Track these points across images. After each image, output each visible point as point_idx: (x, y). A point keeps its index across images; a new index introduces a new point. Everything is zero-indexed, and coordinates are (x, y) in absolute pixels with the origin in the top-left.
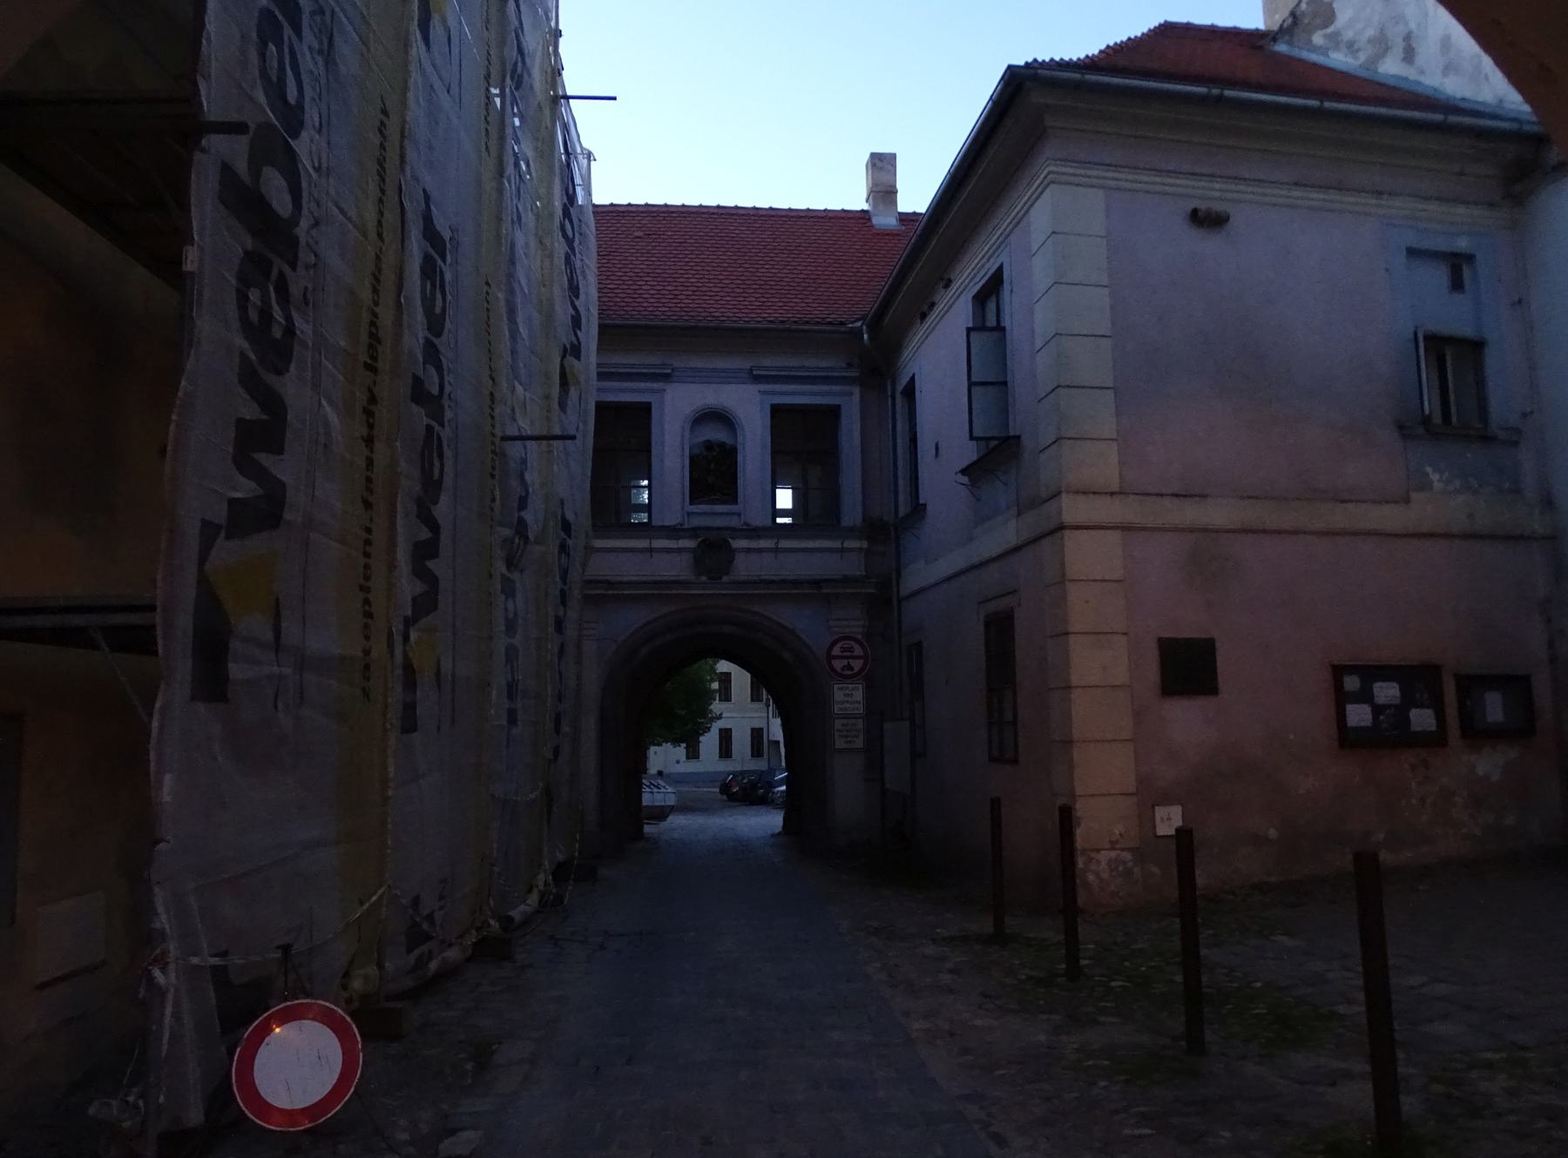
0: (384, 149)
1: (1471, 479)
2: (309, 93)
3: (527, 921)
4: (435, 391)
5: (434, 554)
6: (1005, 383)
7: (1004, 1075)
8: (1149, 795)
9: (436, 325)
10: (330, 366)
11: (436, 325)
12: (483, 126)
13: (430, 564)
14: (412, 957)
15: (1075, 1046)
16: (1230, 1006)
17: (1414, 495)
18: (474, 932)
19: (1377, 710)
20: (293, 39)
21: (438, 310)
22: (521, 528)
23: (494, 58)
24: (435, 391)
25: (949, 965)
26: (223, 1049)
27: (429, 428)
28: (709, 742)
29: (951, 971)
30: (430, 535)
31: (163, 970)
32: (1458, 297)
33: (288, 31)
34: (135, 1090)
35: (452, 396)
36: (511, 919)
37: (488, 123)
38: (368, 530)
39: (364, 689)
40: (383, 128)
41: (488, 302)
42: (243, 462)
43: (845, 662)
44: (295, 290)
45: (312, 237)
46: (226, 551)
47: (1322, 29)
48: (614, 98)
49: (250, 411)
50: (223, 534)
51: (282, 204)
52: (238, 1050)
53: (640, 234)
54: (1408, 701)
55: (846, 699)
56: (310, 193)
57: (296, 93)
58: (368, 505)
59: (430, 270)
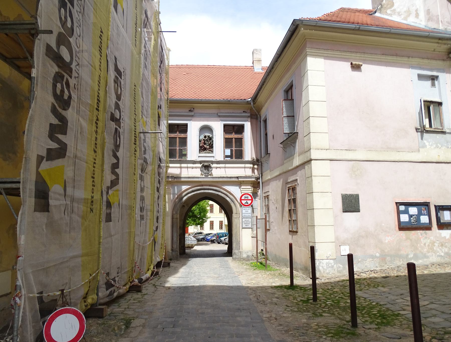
0: (102, 43)
1: (438, 144)
2: (75, 24)
3: (147, 280)
4: (118, 118)
5: (118, 167)
6: (294, 116)
7: (292, 333)
8: (339, 243)
9: (119, 97)
10: (84, 109)
11: (119, 97)
12: (134, 38)
13: (116, 170)
14: (108, 292)
15: (316, 324)
16: (365, 311)
17: (420, 149)
18: (129, 283)
19: (411, 216)
20: (70, 7)
21: (119, 93)
22: (145, 160)
23: (138, 18)
24: (118, 118)
25: (276, 296)
26: (41, 323)
27: (116, 129)
28: (207, 225)
29: (277, 298)
30: (116, 161)
31: (20, 298)
32: (433, 88)
33: (69, 5)
34: (10, 337)
35: (123, 119)
36: (142, 279)
37: (136, 38)
38: (95, 159)
39: (91, 209)
40: (101, 37)
41: (135, 91)
42: (52, 136)
43: (246, 201)
44: (72, 85)
45: (77, 69)
46: (45, 165)
47: (390, 9)
48: (176, 32)
49: (55, 121)
50: (45, 159)
51: (67, 58)
52: (46, 323)
53: (185, 73)
54: (420, 214)
55: (246, 212)
56: (76, 55)
57: (70, 23)
58: (95, 152)
59: (116, 81)
